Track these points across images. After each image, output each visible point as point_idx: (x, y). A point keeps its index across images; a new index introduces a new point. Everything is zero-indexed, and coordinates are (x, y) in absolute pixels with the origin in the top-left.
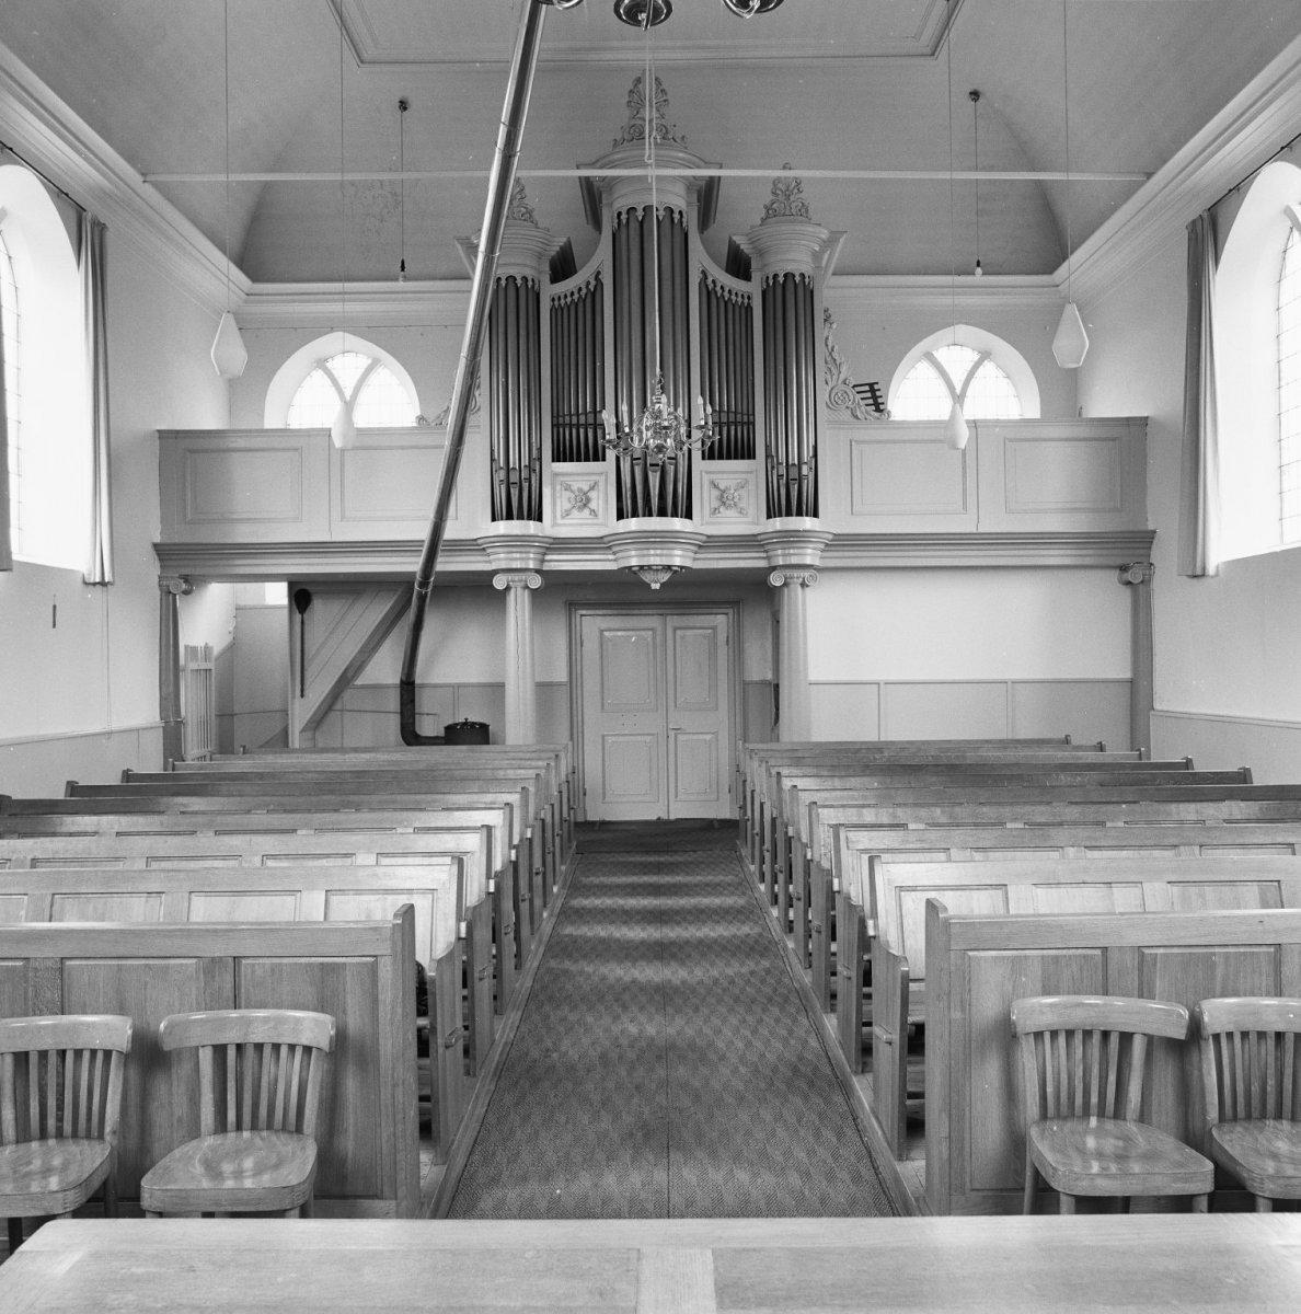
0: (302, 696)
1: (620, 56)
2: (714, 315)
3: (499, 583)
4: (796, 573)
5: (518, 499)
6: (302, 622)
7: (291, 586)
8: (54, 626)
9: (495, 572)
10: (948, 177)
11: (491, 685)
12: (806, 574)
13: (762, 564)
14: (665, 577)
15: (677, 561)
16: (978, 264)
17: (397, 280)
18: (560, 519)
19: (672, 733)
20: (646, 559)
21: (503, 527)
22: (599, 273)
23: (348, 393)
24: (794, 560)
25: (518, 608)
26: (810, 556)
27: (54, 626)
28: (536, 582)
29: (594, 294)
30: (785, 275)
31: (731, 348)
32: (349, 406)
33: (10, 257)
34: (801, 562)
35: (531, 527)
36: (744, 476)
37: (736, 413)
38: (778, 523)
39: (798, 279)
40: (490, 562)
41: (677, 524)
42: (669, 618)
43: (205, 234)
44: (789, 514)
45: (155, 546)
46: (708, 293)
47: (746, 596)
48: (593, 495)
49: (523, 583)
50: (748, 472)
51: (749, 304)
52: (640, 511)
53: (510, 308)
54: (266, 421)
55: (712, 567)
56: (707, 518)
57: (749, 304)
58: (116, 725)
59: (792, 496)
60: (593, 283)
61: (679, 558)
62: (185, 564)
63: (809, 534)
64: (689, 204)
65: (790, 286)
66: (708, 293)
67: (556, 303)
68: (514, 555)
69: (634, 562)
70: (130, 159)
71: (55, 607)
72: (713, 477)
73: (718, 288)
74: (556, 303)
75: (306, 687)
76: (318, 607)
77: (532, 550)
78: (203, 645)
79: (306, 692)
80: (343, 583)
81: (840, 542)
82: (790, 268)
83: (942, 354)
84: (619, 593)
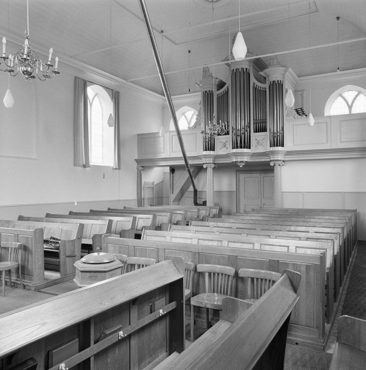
0: (172, 193)
1: (234, 30)
2: (257, 94)
3: (205, 166)
4: (276, 162)
5: (210, 146)
6: (173, 176)
7: (170, 167)
8: (104, 178)
9: (204, 164)
10: (311, 47)
11: (229, 191)
12: (280, 162)
13: (269, 160)
14: (243, 164)
15: (245, 160)
16: (338, 69)
17: (188, 93)
18: (220, 150)
19: (262, 205)
20: (237, 159)
21: (235, 150)
22: (228, 87)
23: (350, 103)
24: (275, 159)
25: (210, 171)
26: (280, 157)
27: (104, 178)
28: (213, 166)
29: (227, 92)
30: (273, 81)
31: (261, 102)
32: (350, 107)
33: (100, 102)
34: (277, 159)
35: (212, 153)
36: (263, 136)
37: (261, 119)
38: (272, 149)
39: (276, 82)
40: (202, 161)
41: (246, 150)
42: (262, 174)
43: (150, 90)
44: (274, 146)
45: (136, 160)
46: (255, 89)
47: (265, 168)
48: (227, 143)
49: (278, 164)
50: (265, 135)
51: (266, 90)
52: (236, 148)
53: (208, 97)
54: (170, 129)
55: (267, 160)
56: (254, 148)
57: (266, 90)
58: (121, 199)
59: (278, 141)
60: (227, 90)
61: (246, 159)
62: (144, 165)
63: (280, 151)
64: (250, 66)
65: (275, 84)
66: (255, 89)
67: (218, 96)
68: (207, 160)
69: (234, 160)
70: (124, 79)
71: (104, 174)
72: (256, 137)
73: (258, 87)
74: (218, 96)
75: (173, 191)
76: (177, 173)
77: (211, 158)
78: (152, 182)
79: (173, 192)
80: (178, 167)
81: (288, 153)
82: (274, 79)
83: (346, 95)
84: (232, 167)
